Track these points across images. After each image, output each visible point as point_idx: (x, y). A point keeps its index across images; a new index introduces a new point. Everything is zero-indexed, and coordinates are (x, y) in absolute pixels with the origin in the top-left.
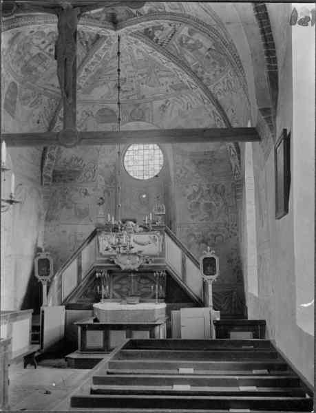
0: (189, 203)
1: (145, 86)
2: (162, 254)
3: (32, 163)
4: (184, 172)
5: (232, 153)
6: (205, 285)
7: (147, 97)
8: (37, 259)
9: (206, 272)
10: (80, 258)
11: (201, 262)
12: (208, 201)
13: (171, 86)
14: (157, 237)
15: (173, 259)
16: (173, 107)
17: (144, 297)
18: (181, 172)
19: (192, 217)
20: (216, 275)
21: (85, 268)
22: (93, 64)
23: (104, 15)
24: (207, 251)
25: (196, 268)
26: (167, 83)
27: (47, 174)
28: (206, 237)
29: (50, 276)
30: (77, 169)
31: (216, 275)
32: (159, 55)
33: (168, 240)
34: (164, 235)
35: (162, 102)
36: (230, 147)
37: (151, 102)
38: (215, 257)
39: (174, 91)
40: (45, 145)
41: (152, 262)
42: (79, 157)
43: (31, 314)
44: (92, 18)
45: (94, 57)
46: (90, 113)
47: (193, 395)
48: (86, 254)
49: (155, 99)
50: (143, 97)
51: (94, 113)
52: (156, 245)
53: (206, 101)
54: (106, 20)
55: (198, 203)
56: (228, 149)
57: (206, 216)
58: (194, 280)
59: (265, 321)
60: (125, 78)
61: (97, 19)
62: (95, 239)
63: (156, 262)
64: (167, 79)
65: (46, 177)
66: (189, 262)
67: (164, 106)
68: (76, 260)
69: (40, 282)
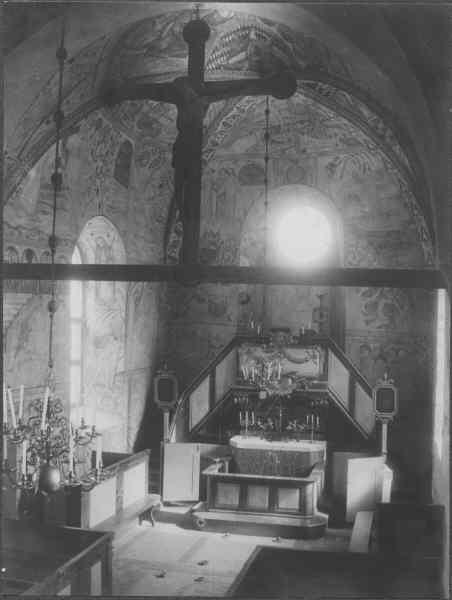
0: (364, 303)
1: (306, 136)
2: (324, 376)
3: (153, 242)
4: (358, 258)
5: (425, 236)
6: (378, 425)
7: (309, 151)
8: (156, 380)
9: (380, 408)
10: (213, 376)
11: (374, 392)
12: (389, 302)
13: (341, 140)
14: (317, 354)
15: (338, 382)
16: (344, 168)
17: (305, 435)
18: (354, 258)
19: (367, 323)
20: (393, 413)
21: (220, 392)
22: (234, 117)
23: (246, 65)
24: (384, 379)
25: (368, 397)
26: (336, 135)
27: (173, 254)
28: (385, 350)
29: (174, 402)
30: (213, 248)
31: (393, 413)
32: (324, 108)
33: (333, 358)
34: (327, 352)
35: (329, 160)
36: (422, 228)
37: (315, 159)
38: (393, 388)
39: (345, 146)
40: (155, 580)
41: (310, 388)
42: (215, 231)
43: (147, 457)
44: (231, 69)
45: (235, 109)
46: (230, 171)
47: (238, 524)
48: (222, 372)
49: (322, 154)
50: (304, 151)
51: (237, 172)
52: (316, 363)
53: (389, 166)
54: (251, 69)
55: (375, 305)
56: (419, 230)
57: (386, 322)
58: (366, 412)
59: (149, 492)
60: (279, 126)
61: (239, 69)
62: (231, 355)
63: (315, 386)
64: (336, 130)
65: (170, 257)
66: (360, 391)
67: (332, 166)
68: (208, 379)
69: (161, 410)
